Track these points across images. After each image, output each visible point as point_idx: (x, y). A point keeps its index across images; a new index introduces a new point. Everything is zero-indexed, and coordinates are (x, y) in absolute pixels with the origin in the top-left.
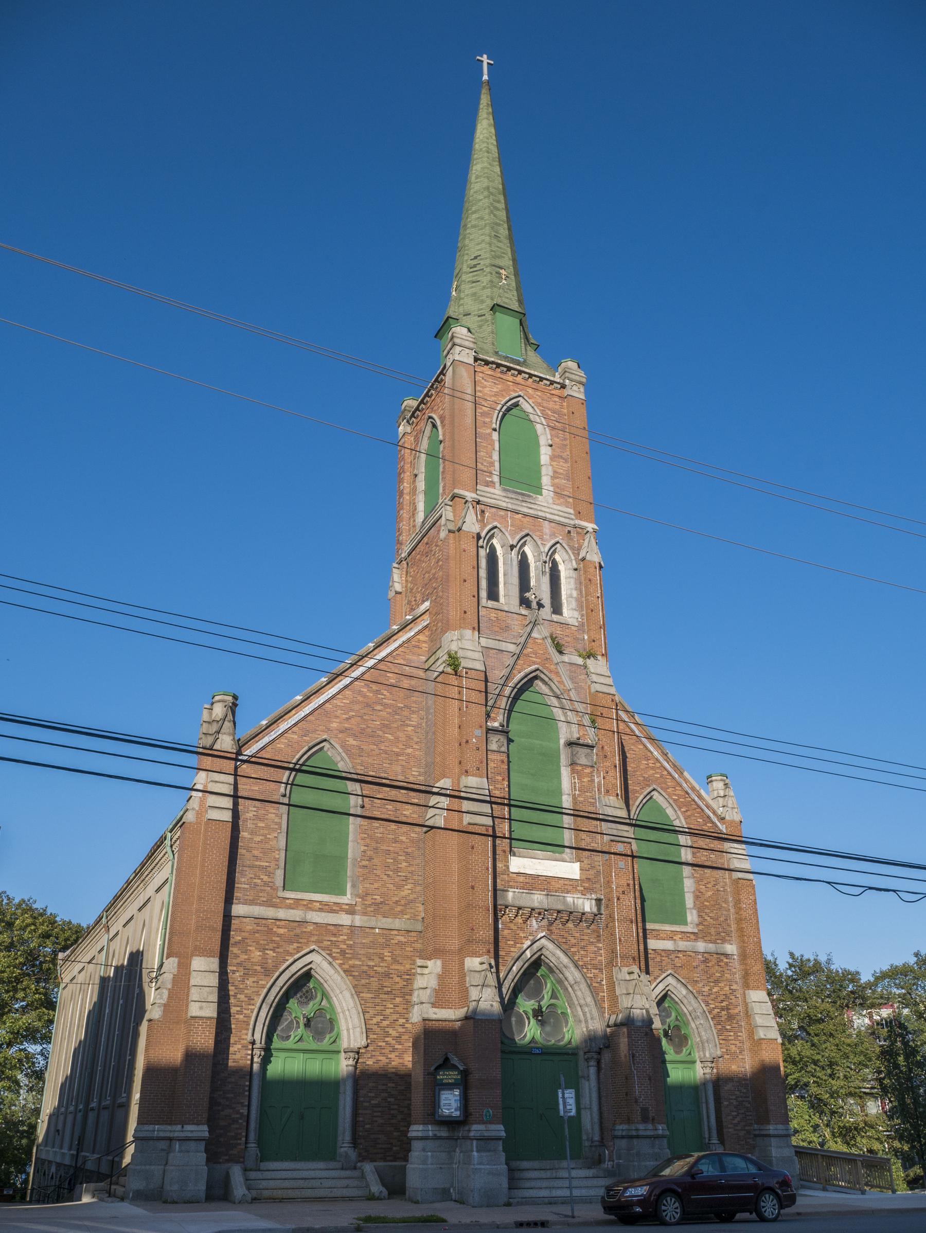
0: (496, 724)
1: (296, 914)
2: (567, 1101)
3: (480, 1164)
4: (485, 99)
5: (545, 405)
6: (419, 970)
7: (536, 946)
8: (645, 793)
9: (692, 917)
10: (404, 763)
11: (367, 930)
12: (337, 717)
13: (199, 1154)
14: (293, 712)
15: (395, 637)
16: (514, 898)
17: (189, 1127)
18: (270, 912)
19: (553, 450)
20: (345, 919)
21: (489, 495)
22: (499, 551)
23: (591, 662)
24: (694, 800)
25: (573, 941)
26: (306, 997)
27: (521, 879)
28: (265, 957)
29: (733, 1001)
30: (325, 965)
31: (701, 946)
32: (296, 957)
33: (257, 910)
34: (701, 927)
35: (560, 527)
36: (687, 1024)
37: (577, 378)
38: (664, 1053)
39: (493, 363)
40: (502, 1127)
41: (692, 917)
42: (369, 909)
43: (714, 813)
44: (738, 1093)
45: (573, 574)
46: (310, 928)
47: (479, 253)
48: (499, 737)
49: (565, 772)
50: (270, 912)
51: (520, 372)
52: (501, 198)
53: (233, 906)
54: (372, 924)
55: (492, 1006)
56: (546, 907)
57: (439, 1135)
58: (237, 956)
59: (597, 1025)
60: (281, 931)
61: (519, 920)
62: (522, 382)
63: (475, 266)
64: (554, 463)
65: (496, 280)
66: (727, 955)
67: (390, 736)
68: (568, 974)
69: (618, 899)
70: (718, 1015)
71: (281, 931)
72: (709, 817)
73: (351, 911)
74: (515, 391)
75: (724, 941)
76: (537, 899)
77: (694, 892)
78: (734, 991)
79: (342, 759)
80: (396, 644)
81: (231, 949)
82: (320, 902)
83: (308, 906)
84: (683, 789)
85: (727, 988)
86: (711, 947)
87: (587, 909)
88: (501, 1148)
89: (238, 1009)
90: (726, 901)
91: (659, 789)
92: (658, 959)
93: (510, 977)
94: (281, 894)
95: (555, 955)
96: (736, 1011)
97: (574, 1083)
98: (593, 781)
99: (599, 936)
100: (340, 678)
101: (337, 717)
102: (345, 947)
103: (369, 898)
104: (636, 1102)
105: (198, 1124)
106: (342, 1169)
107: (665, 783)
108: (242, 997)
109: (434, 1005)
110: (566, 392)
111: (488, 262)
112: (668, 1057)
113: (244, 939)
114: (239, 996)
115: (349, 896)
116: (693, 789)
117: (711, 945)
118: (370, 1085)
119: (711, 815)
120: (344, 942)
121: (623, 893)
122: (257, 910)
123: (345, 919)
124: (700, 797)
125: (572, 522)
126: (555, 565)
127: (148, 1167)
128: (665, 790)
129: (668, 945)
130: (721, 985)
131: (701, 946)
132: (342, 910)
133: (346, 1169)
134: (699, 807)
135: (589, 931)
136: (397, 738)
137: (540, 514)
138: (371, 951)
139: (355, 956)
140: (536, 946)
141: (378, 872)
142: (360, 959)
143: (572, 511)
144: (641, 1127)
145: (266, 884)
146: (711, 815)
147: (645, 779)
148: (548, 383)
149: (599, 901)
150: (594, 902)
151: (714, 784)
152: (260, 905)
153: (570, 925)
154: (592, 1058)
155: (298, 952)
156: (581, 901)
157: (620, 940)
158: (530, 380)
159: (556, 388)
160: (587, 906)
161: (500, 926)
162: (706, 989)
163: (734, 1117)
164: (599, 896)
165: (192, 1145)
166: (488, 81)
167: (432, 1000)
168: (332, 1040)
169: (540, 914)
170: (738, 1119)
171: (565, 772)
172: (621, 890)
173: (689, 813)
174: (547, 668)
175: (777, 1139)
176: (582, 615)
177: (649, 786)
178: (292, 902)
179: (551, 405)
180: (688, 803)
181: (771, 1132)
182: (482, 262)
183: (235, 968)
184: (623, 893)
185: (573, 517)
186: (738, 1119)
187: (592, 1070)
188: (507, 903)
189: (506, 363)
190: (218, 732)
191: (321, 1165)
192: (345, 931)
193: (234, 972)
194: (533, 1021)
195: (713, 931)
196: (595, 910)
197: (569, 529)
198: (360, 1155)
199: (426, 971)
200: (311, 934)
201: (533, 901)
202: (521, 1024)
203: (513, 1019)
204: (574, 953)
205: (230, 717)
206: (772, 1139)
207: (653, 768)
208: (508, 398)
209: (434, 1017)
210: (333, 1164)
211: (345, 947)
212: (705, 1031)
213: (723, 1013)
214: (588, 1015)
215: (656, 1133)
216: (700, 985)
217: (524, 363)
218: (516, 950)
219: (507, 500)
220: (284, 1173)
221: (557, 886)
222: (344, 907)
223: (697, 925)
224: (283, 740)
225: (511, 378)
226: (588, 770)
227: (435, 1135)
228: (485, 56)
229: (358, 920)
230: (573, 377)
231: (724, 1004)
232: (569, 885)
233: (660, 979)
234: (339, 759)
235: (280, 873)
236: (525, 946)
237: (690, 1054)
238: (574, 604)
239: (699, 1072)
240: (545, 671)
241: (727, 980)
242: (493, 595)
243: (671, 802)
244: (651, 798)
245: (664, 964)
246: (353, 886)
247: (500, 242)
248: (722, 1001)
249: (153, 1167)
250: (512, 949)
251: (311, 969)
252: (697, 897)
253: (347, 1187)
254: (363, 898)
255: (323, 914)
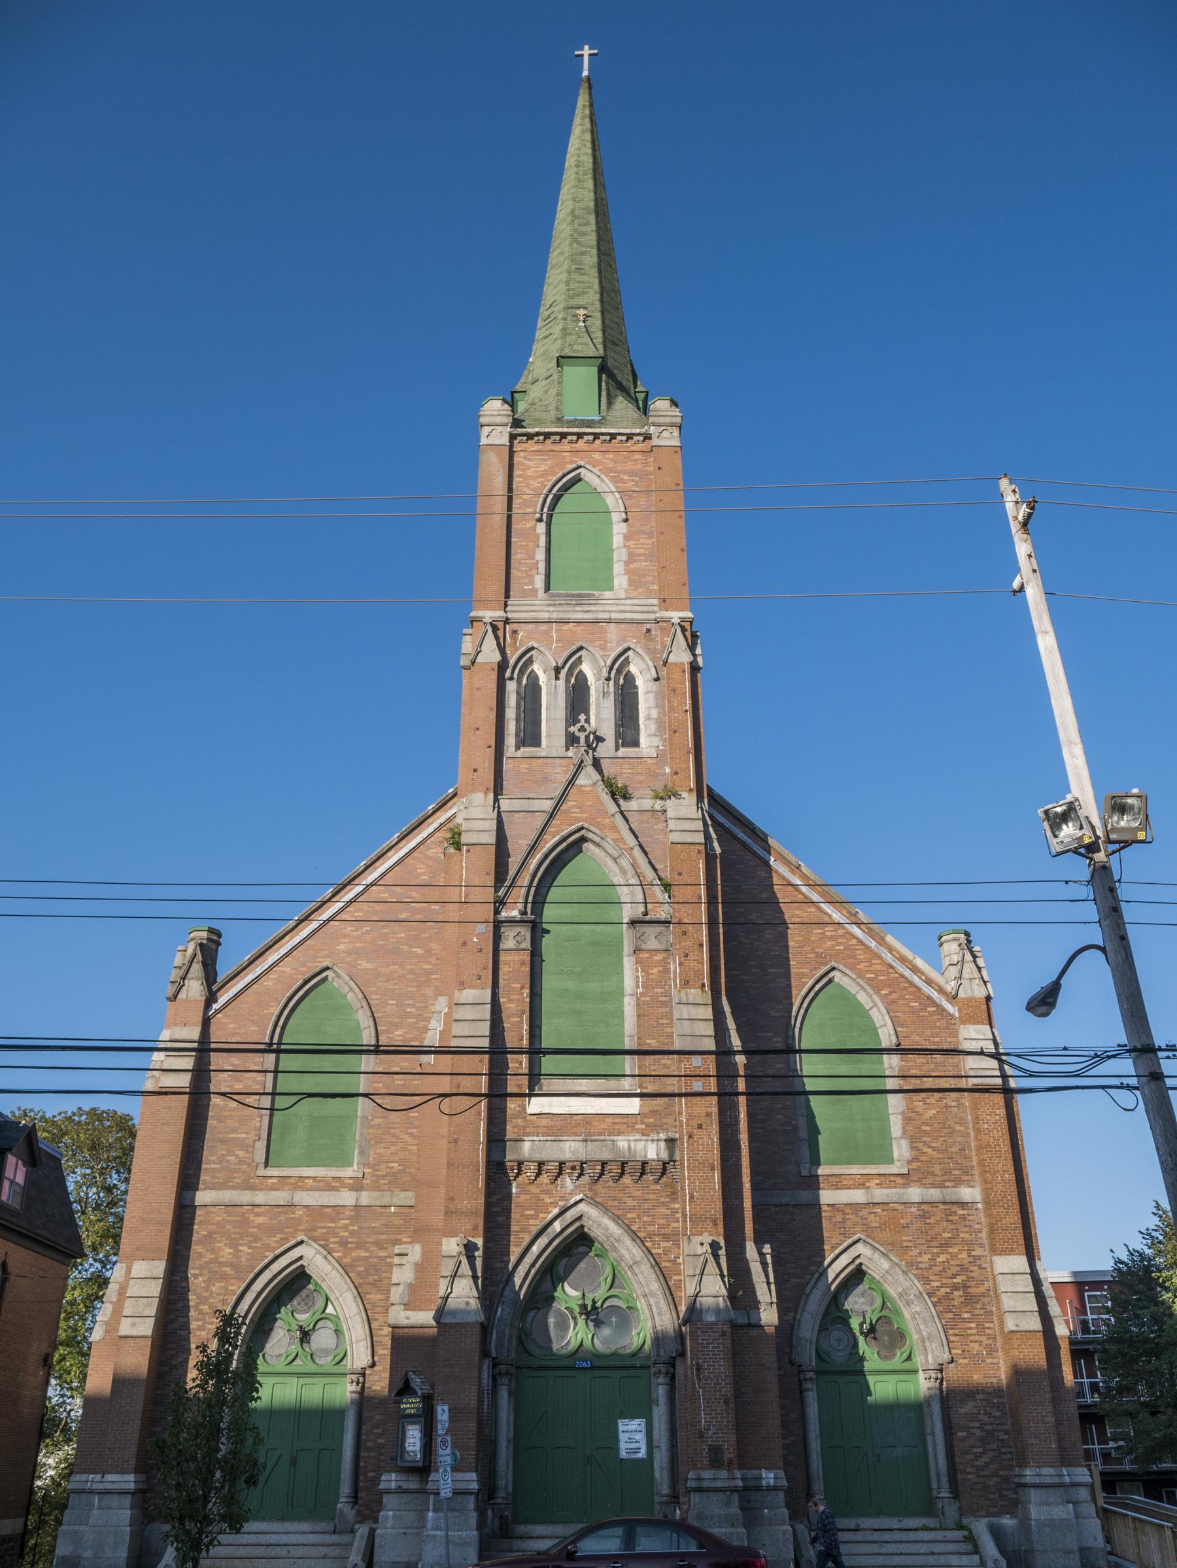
0: (515, 913)
1: (280, 1197)
2: (632, 1436)
3: (437, 1529)
4: (583, 100)
5: (619, 468)
6: (397, 1260)
7: (570, 1216)
8: (817, 976)
9: (901, 1150)
10: (437, 983)
11: (379, 1210)
12: (346, 936)
13: (124, 1511)
14: (287, 938)
15: (430, 820)
16: (532, 1149)
17: (110, 1477)
18: (245, 1197)
19: (630, 526)
20: (347, 1198)
21: (525, 608)
22: (543, 679)
23: (671, 804)
24: (902, 976)
25: (631, 1202)
26: (306, 1304)
27: (544, 1122)
28: (237, 1254)
29: (975, 1274)
30: (319, 1260)
31: (915, 1193)
32: (277, 1252)
33: (228, 1196)
34: (915, 1165)
35: (634, 627)
36: (898, 1312)
37: (668, 420)
38: (862, 1359)
39: (538, 434)
40: (474, 1476)
41: (901, 1150)
42: (382, 1181)
43: (941, 990)
44: (985, 1418)
45: (654, 686)
46: (300, 1212)
47: (554, 298)
48: (519, 929)
49: (628, 963)
50: (245, 1197)
51: (596, 436)
52: (592, 218)
53: (821, 1192)
54: (386, 1200)
55: (468, 1303)
56: (583, 1157)
57: (405, 1486)
58: (201, 1255)
59: (666, 1321)
60: (261, 1220)
61: (544, 1179)
62: (586, 447)
63: (549, 316)
64: (631, 543)
65: (570, 325)
66: (963, 1205)
67: (419, 951)
68: (624, 1252)
69: (690, 1137)
70: (947, 1297)
71: (261, 1220)
72: (929, 998)
73: (357, 1185)
74: (572, 462)
75: (958, 1182)
76: (570, 1148)
77: (903, 1113)
78: (979, 1258)
79: (351, 989)
80: (431, 829)
81: (193, 1247)
82: (314, 1178)
83: (299, 1184)
84: (884, 962)
85: (964, 1255)
86: (934, 1194)
87: (652, 1154)
88: (472, 1506)
89: (200, 1323)
90: (962, 1122)
91: (841, 967)
92: (839, 1218)
93: (528, 1260)
94: (261, 1172)
95: (600, 1224)
96: (982, 1289)
97: (643, 1410)
98: (667, 971)
99: (674, 1193)
100: (349, 887)
101: (346, 936)
102: (346, 1234)
103: (382, 1167)
104: (701, 1436)
105: (123, 1473)
106: (334, 1532)
107: (854, 956)
108: (205, 1308)
109: (407, 1306)
110: (655, 441)
111: (561, 306)
112: (867, 1366)
113: (210, 1235)
114: (201, 1307)
115: (355, 1167)
116: (903, 960)
117: (932, 1191)
118: (377, 1417)
119: (935, 995)
120: (345, 1227)
121: (700, 1127)
122: (228, 1196)
123: (347, 1198)
124: (915, 970)
125: (652, 616)
126: (630, 679)
127: (77, 1527)
128: (852, 967)
129: (858, 1196)
130: (955, 1250)
131: (915, 1193)
132: (344, 1185)
133: (340, 1533)
134: (912, 984)
135: (658, 1187)
136: (429, 952)
137: (601, 616)
138: (384, 1237)
139: (361, 1245)
140: (570, 1216)
141: (397, 1131)
142: (367, 1250)
143: (655, 602)
144: (707, 1474)
145: (241, 1161)
146: (935, 995)
147: (819, 955)
148: (624, 438)
149: (671, 1142)
150: (663, 1144)
151: (945, 946)
152: (234, 1188)
153: (627, 1180)
154: (660, 1372)
155: (282, 1245)
156: (641, 1145)
157: (692, 1197)
158: (597, 442)
159: (638, 442)
160: (653, 1151)
161: (514, 1190)
162: (925, 1258)
163: (978, 1457)
164: (671, 1135)
165: (114, 1500)
166: (588, 79)
167: (405, 1300)
168: (905, 1356)
169: (573, 1168)
170: (985, 1459)
171: (628, 963)
172: (695, 1123)
173: (894, 996)
174: (598, 825)
175: (1043, 1491)
176: (664, 741)
177: (825, 964)
178: (275, 1181)
179: (630, 466)
180: (893, 986)
181: (1028, 1480)
182: (556, 309)
183: (197, 1272)
184: (700, 1127)
185: (656, 609)
186: (985, 1459)
187: (661, 1392)
188: (521, 1158)
189: (557, 430)
190: (184, 978)
191: (305, 1526)
192: (348, 1213)
193: (196, 1276)
194: (581, 1320)
195: (937, 1169)
196: (665, 1155)
197: (648, 626)
198: (359, 1513)
199: (404, 1260)
200: (299, 1221)
201: (563, 1151)
202: (563, 1326)
203: (551, 1320)
204: (633, 1220)
205: (968, 957)
206: (1032, 1491)
207: (831, 938)
208: (560, 474)
209: (405, 1322)
210: (321, 1526)
211: (346, 1234)
212: (925, 1323)
213: (956, 1293)
214: (654, 1310)
215: (732, 1483)
216: (914, 1253)
217: (600, 423)
218: (537, 1222)
219: (551, 609)
220: (925, 1538)
221: (603, 1126)
222: (347, 1181)
223: (909, 1162)
224: (271, 975)
225: (568, 447)
226: (659, 957)
227: (399, 1487)
228: (586, 47)
229: (365, 1198)
230: (661, 420)
231: (958, 1280)
232: (625, 1123)
233: (841, 1248)
234: (347, 989)
235: (261, 1146)
236: (550, 1216)
237: (909, 1358)
238: (653, 727)
239: (923, 1385)
240: (592, 828)
241: (964, 1241)
242: (530, 736)
243: (862, 983)
244: (830, 981)
245: (848, 1224)
246: (361, 1153)
247: (584, 274)
248: (955, 1276)
249: (82, 1528)
250: (531, 1222)
251: (861, 1264)
252: (907, 1120)
253: (324, 1557)
254: (374, 1167)
255: (317, 1194)
